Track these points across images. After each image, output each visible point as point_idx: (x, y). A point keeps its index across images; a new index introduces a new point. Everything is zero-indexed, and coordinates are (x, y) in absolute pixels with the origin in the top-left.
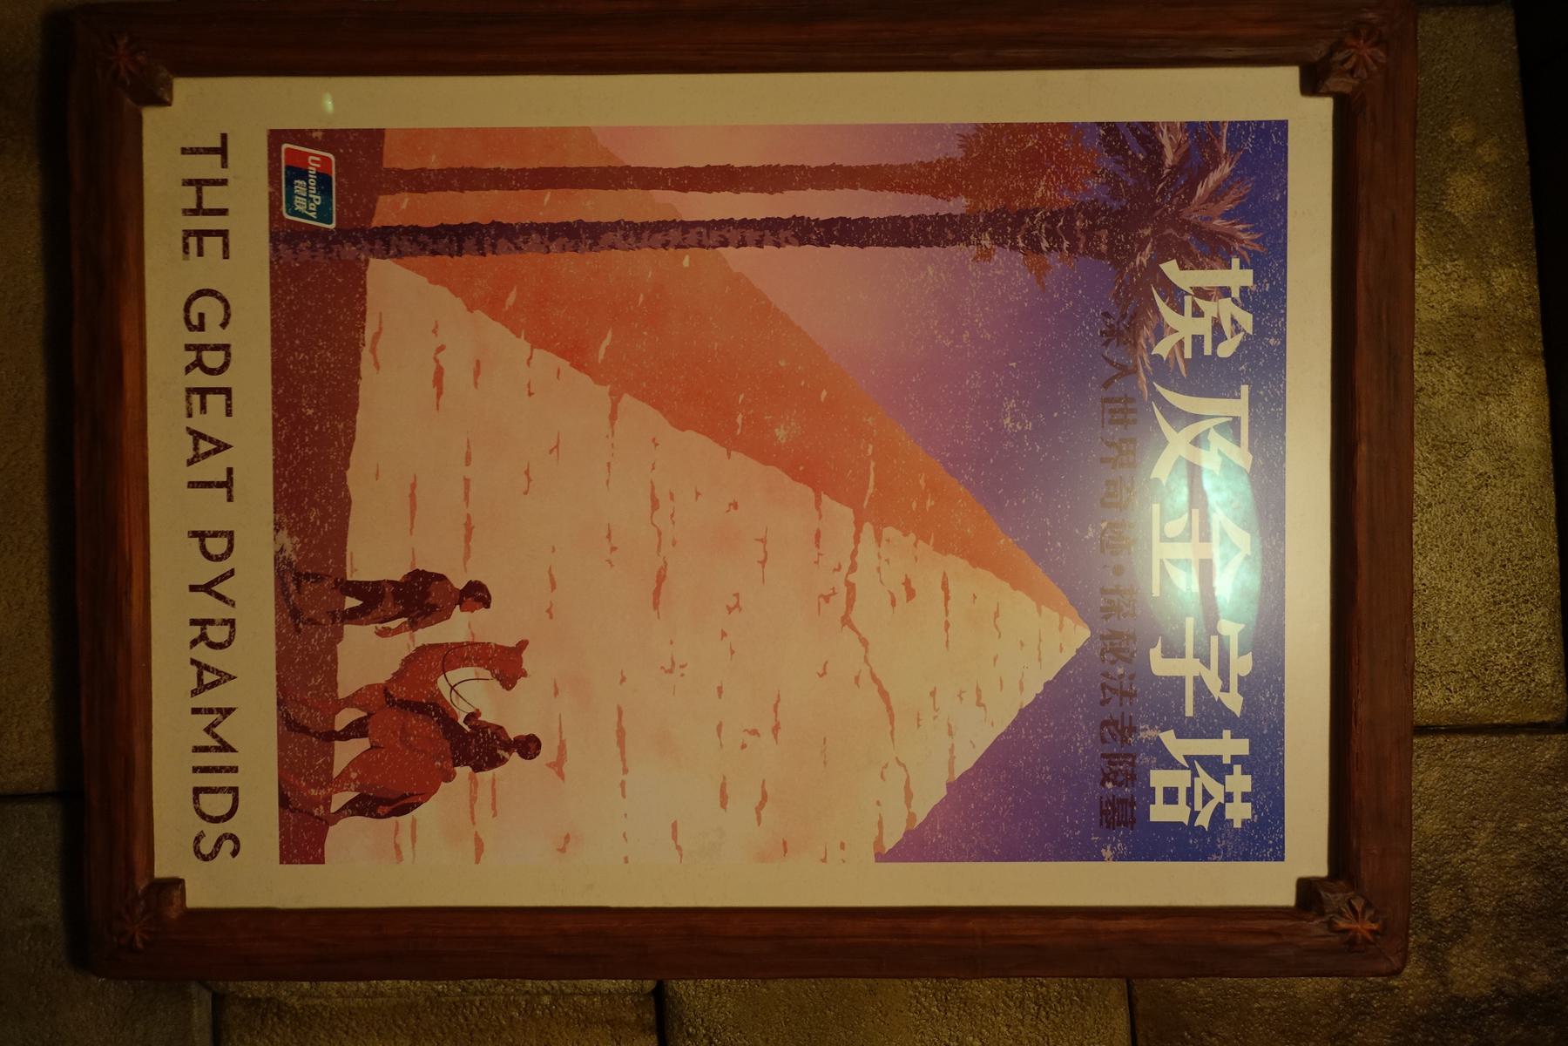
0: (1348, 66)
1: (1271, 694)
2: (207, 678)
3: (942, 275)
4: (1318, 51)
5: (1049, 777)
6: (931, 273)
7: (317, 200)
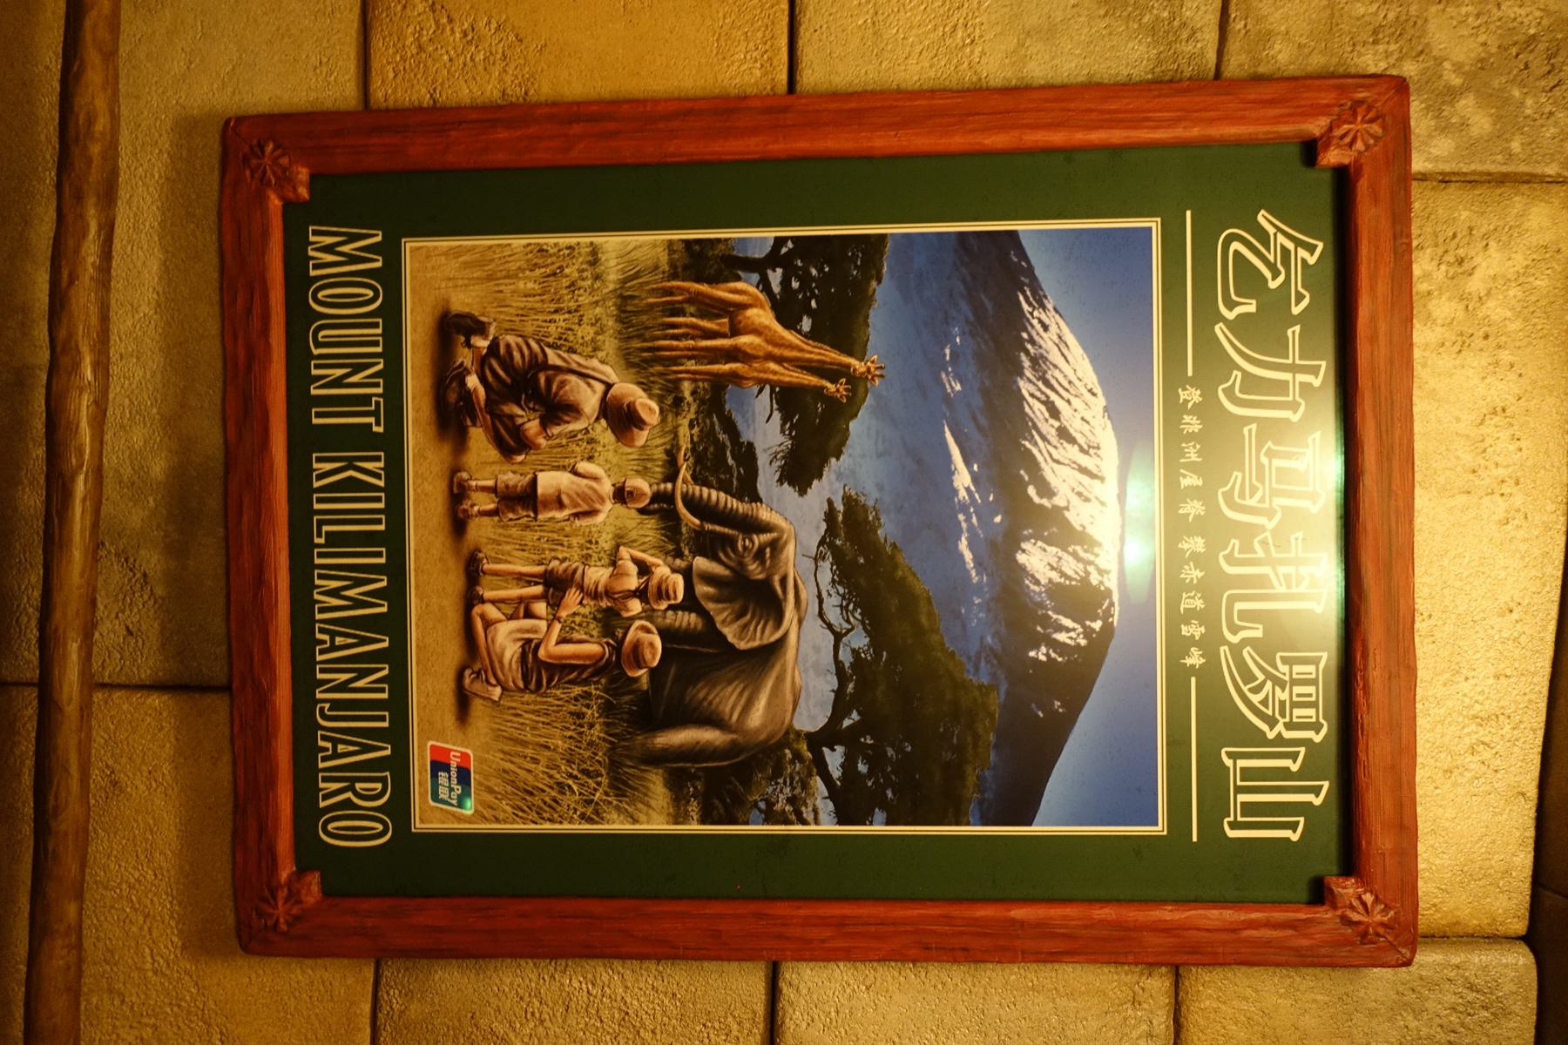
0: (1348, 140)
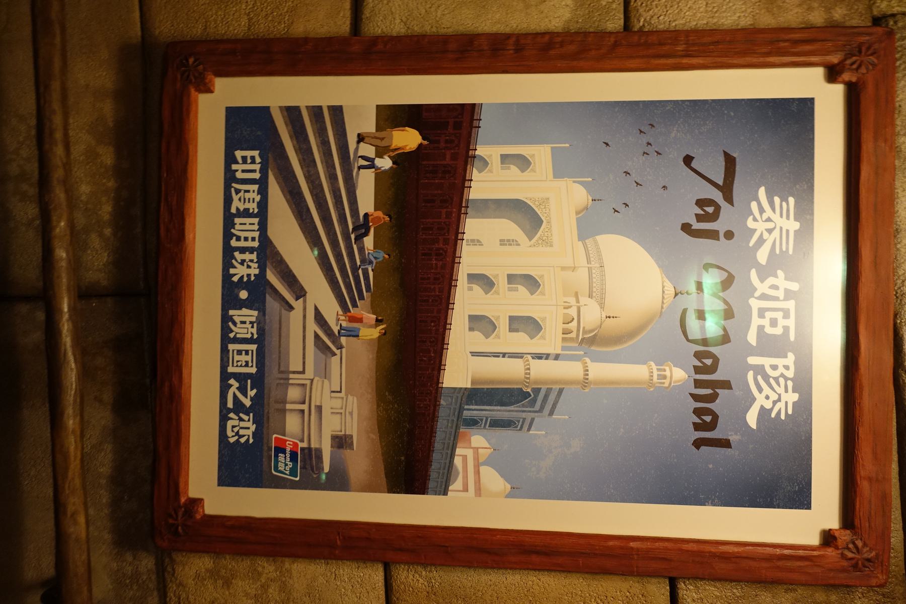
0: (855, 66)
1: (806, 417)
2: (246, 239)
3: (618, 179)
4: (835, 59)
5: (675, 460)
6: (611, 178)
7: (290, 465)
